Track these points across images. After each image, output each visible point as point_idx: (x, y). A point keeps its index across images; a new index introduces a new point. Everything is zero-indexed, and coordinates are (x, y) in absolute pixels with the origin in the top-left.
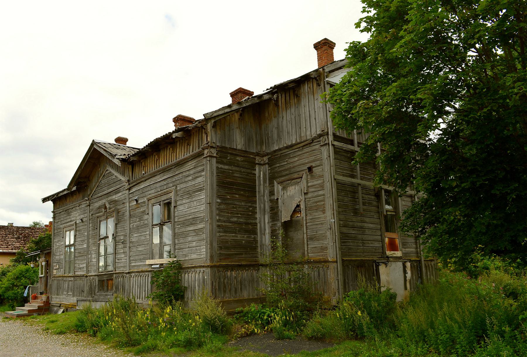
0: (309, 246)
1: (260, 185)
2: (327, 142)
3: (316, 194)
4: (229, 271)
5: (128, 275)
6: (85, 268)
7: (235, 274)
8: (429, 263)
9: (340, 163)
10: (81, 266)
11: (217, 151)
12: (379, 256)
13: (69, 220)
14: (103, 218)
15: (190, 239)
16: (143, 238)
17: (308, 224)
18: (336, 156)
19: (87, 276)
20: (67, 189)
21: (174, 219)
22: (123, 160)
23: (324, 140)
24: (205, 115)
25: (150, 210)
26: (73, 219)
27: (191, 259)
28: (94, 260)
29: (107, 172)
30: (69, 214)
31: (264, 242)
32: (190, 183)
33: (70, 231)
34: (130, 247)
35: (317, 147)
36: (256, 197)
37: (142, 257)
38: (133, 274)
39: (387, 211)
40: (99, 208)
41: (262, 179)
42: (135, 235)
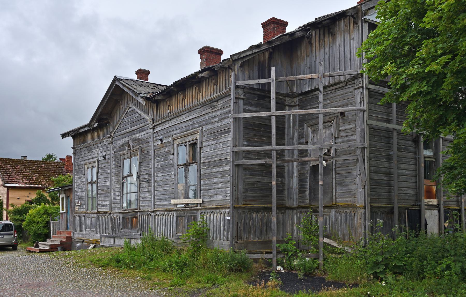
1: (289, 127)
3: (346, 139)
4: (255, 213)
5: (152, 214)
7: (260, 216)
11: (244, 92)
12: (412, 204)
14: (126, 156)
15: (216, 180)
16: (168, 178)
17: (337, 169)
19: (110, 214)
20: (89, 125)
22: (147, 99)
23: (358, 83)
26: (94, 156)
29: (130, 110)
30: (90, 151)
31: (291, 185)
34: (154, 187)
35: (351, 90)
36: (285, 139)
37: (167, 197)
39: (425, 158)
40: (123, 145)
41: (291, 121)
42: (160, 175)
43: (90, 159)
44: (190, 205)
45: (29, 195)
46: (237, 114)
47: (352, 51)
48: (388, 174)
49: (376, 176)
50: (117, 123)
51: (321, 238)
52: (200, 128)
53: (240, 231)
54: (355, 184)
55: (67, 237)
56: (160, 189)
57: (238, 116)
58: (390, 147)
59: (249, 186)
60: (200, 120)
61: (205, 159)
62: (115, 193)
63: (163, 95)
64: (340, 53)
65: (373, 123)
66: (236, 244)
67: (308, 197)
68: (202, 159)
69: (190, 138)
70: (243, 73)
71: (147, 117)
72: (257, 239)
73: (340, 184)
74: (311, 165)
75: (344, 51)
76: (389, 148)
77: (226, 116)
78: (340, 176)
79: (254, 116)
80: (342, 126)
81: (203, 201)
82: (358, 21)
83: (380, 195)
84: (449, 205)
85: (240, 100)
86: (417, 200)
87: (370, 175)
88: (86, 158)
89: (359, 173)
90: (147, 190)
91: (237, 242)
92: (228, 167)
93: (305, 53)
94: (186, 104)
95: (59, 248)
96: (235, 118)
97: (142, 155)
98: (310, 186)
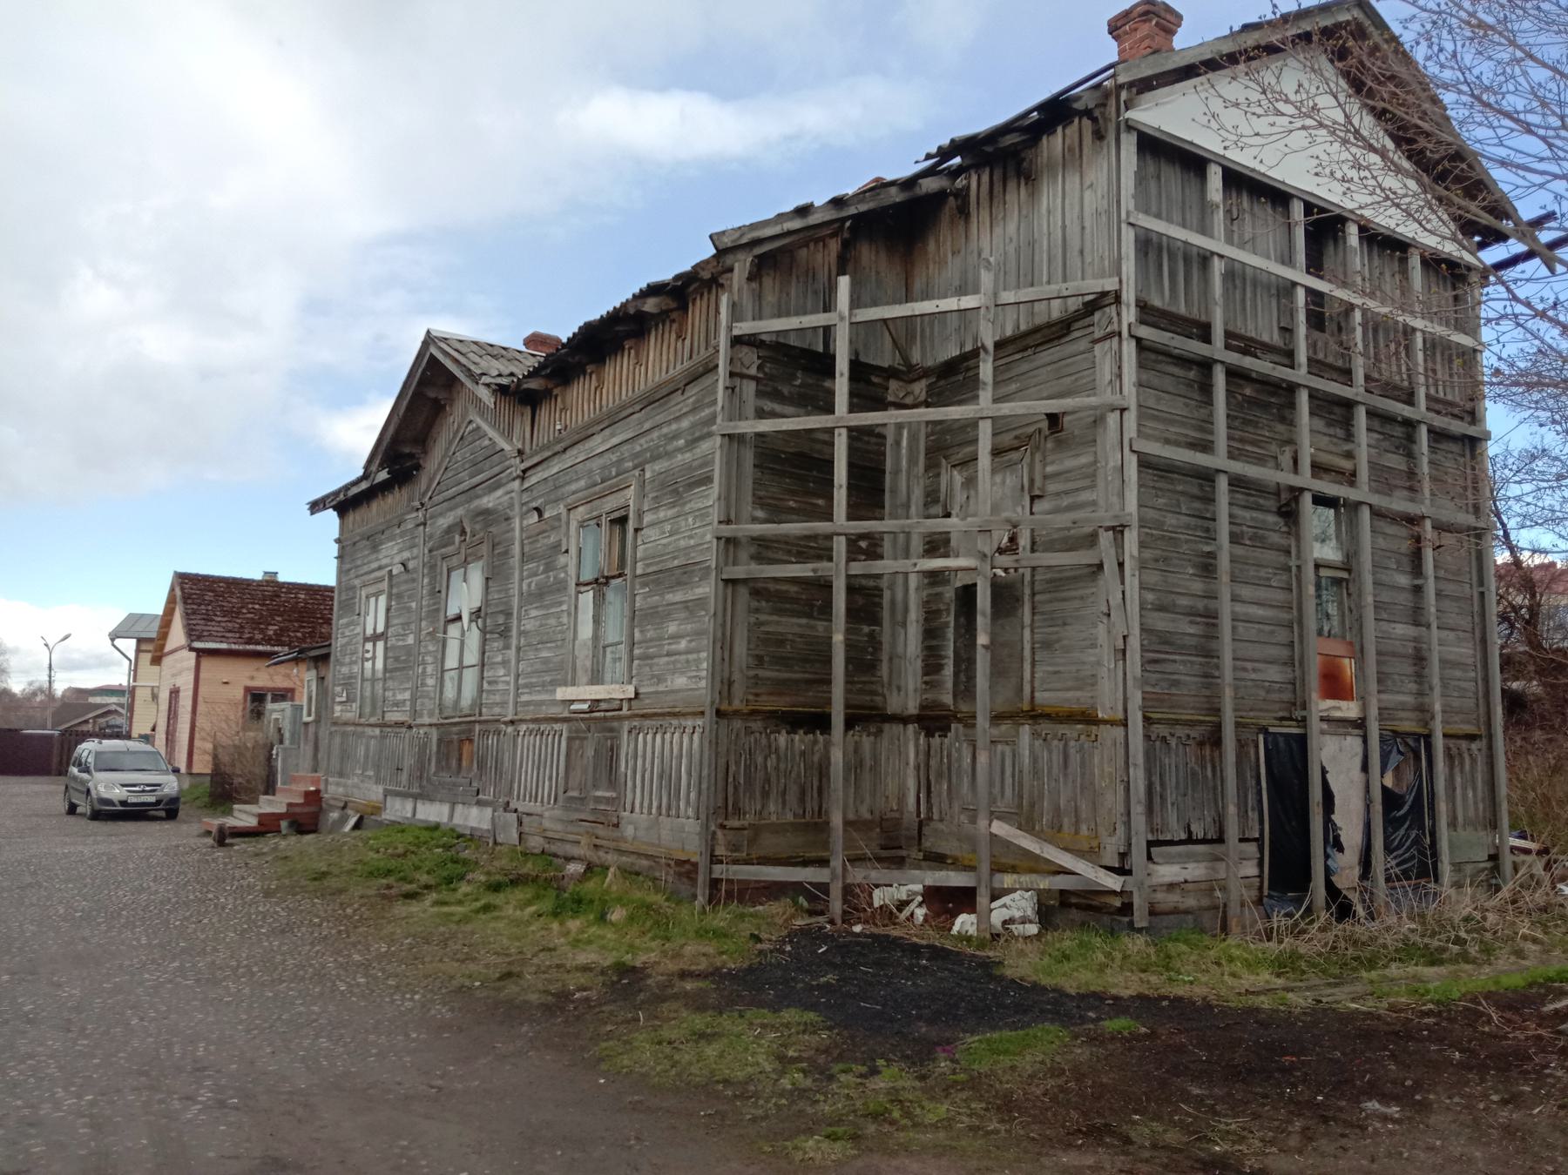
0: (1038, 669)
1: (897, 472)
2: (1115, 327)
3: (1066, 501)
4: (784, 732)
5: (510, 729)
6: (408, 703)
7: (802, 741)
8: (1464, 744)
9: (1159, 399)
10: (400, 697)
11: (759, 358)
12: (1281, 714)
13: (374, 565)
14: (455, 561)
15: (672, 628)
16: (552, 621)
17: (1037, 598)
18: (1144, 377)
19: (410, 727)
20: (365, 477)
21: (634, 569)
22: (502, 390)
23: (1104, 322)
24: (715, 238)
25: (573, 541)
26: (384, 562)
27: (672, 692)
28: (430, 682)
29: (470, 427)
30: (375, 548)
31: (900, 650)
32: (680, 458)
33: (377, 595)
34: (519, 649)
35: (1083, 345)
36: (883, 507)
37: (548, 679)
38: (523, 727)
39: (1317, 566)
40: (449, 530)
41: (904, 451)
42: (534, 613)
43: (373, 571)
44: (603, 706)
45: (255, 674)
46: (732, 424)
47: (1087, 224)
48: (1200, 616)
49: (1161, 622)
50: (439, 469)
51: (982, 823)
52: (637, 473)
53: (736, 788)
54: (1094, 646)
55: (307, 794)
56: (531, 655)
57: (735, 427)
58: (1207, 530)
59: (769, 649)
60: (638, 448)
61: (648, 565)
62: (424, 669)
63: (543, 376)
64: (1049, 234)
65: (1154, 449)
66: (719, 833)
67: (949, 685)
68: (639, 564)
69: (611, 503)
70: (759, 297)
71: (507, 447)
72: (790, 817)
73: (1047, 645)
74: (958, 584)
75: (1064, 227)
76: (1209, 534)
77: (705, 430)
78: (1045, 620)
79: (784, 428)
80: (1052, 463)
81: (637, 694)
82: (1106, 130)
83: (1176, 683)
84: (1393, 720)
85: (745, 381)
86: (1294, 704)
87: (1141, 616)
88: (366, 569)
89: (1106, 610)
90: (499, 659)
91: (723, 827)
92: (706, 589)
93: (949, 244)
94: (604, 402)
95: (284, 824)
96: (729, 435)
97: (493, 556)
98: (955, 652)
